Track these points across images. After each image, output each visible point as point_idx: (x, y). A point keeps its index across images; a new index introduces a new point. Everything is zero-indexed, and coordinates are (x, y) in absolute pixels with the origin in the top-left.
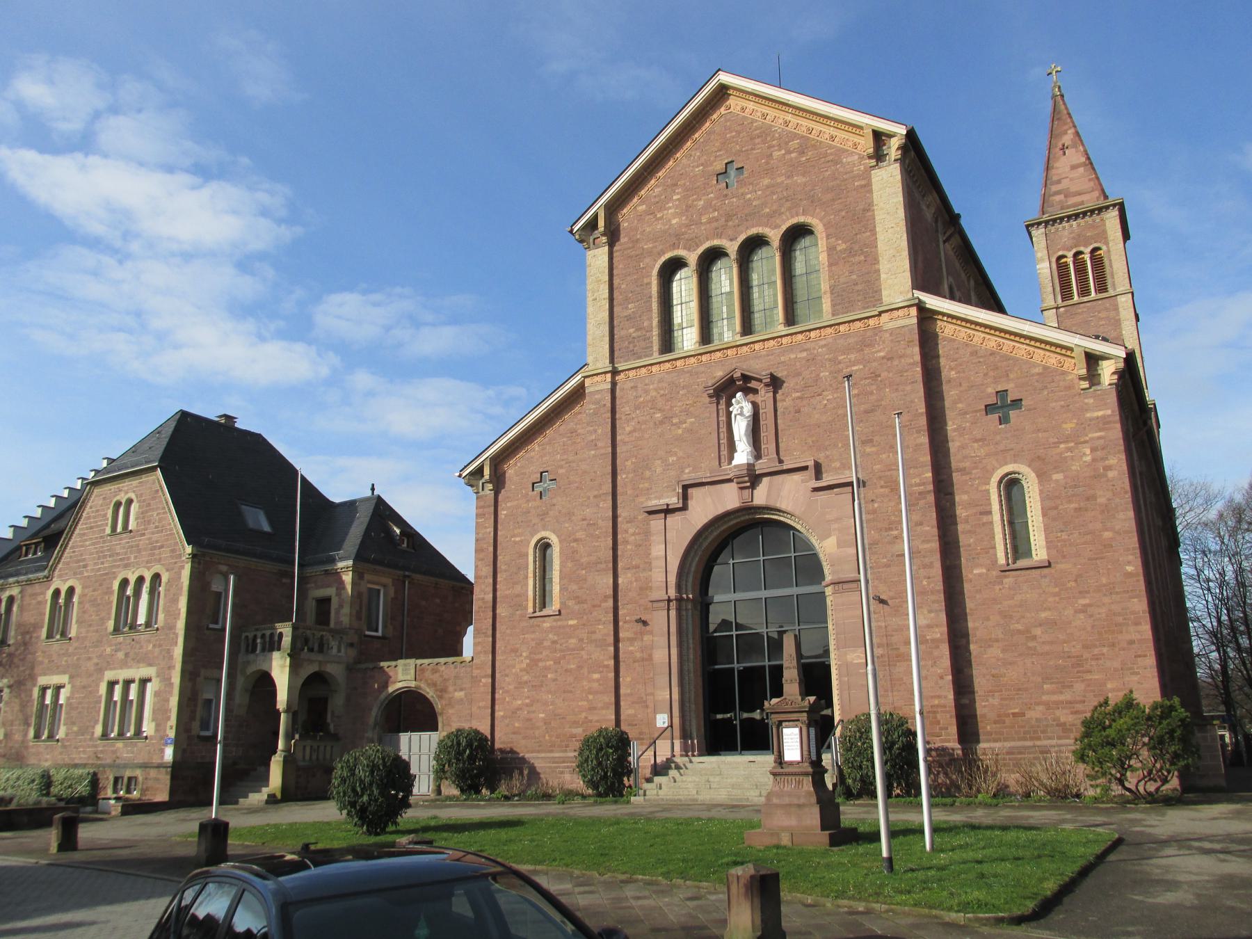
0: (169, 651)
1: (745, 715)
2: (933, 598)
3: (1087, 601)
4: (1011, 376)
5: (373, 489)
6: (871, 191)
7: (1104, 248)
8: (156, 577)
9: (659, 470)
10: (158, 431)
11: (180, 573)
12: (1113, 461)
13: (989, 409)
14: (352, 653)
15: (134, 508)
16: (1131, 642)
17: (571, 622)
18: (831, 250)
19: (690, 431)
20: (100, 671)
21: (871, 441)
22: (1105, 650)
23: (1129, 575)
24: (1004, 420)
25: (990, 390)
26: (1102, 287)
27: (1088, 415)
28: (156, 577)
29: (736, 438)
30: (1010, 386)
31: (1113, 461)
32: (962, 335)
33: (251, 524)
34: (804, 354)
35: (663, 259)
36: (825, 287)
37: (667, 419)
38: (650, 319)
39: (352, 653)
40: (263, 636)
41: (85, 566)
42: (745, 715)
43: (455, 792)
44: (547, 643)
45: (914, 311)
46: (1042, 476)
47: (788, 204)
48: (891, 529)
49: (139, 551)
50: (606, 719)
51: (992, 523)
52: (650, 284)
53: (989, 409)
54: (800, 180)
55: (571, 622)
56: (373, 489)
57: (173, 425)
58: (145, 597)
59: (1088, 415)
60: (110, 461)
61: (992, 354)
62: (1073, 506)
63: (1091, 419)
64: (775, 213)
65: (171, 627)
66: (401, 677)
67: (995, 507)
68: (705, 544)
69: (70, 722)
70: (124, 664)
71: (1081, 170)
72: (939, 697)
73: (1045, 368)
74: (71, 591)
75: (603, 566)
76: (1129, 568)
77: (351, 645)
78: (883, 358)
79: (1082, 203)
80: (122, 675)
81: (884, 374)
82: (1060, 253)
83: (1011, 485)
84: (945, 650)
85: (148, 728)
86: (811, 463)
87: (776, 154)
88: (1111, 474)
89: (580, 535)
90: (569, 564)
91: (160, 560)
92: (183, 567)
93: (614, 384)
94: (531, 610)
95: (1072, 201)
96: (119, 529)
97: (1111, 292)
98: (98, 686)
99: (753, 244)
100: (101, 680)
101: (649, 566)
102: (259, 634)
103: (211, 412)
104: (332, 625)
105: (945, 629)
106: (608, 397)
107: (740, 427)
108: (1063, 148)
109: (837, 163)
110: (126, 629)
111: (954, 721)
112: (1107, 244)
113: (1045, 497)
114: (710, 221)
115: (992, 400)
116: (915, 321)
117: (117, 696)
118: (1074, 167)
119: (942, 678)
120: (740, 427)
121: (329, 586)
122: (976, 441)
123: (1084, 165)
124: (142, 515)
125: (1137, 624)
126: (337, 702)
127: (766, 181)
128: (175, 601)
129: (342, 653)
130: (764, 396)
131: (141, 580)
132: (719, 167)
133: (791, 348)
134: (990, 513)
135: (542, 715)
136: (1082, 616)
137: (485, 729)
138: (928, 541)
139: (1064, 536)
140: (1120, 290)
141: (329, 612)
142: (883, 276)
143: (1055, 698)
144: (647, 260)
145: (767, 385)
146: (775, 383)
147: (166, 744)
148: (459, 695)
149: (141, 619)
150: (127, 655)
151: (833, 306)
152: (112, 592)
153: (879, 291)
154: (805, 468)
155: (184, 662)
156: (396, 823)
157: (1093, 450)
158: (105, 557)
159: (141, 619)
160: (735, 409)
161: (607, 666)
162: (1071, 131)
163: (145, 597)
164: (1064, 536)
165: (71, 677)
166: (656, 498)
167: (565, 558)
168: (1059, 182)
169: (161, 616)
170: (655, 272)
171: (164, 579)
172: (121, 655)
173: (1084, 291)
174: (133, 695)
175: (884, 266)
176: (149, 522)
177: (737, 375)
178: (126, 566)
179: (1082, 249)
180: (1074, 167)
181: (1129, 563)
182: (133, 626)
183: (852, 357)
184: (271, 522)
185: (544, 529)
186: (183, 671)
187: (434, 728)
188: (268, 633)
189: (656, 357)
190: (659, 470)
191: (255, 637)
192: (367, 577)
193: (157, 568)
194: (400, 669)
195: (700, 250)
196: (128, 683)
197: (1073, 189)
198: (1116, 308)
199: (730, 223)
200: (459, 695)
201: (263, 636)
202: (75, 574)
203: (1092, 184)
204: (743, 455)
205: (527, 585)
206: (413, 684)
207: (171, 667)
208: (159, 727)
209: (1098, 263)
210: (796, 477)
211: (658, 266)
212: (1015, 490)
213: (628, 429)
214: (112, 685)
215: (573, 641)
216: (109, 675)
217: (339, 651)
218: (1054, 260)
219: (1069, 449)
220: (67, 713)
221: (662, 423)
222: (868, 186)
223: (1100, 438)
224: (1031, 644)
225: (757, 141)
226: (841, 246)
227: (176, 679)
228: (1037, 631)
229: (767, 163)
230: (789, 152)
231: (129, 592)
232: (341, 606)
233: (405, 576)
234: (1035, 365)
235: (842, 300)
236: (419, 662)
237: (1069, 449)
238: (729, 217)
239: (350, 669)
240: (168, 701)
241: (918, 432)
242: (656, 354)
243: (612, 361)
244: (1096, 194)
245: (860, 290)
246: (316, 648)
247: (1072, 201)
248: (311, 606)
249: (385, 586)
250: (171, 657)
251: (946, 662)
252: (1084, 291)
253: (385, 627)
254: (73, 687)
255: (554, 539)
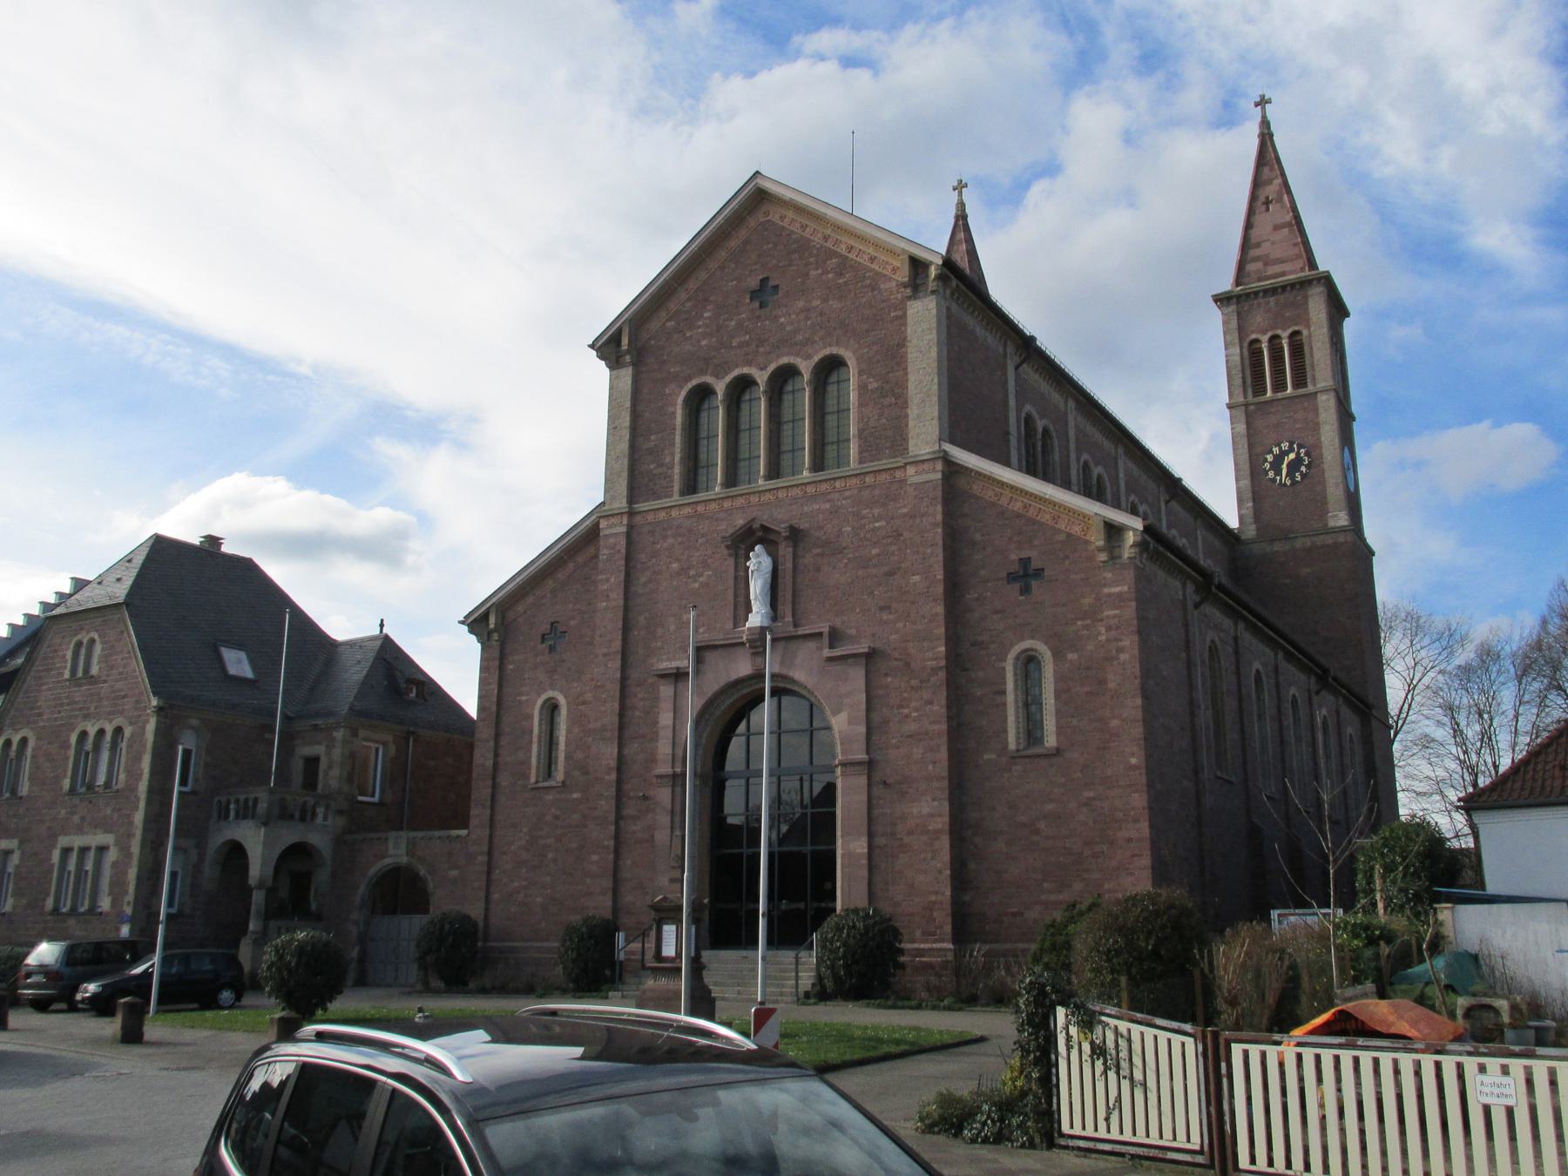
0: (128, 816)
1: (802, 905)
2: (936, 784)
3: (1091, 794)
4: (1036, 543)
5: (382, 625)
6: (905, 324)
7: (1305, 332)
8: (118, 731)
9: (672, 628)
10: (129, 559)
11: (144, 728)
12: (1126, 643)
13: (1012, 578)
14: (341, 822)
15: (98, 648)
16: (1129, 840)
17: (575, 796)
18: (862, 388)
19: (705, 585)
20: (53, 837)
21: (889, 607)
22: (1105, 848)
23: (1134, 768)
24: (1026, 590)
25: (1013, 557)
26: (1300, 380)
27: (1106, 590)
28: (118, 731)
29: (752, 597)
30: (1033, 554)
31: (1126, 643)
32: (991, 493)
33: (243, 655)
34: (828, 505)
35: (690, 386)
36: (853, 430)
37: (684, 570)
38: (673, 454)
39: (341, 822)
40: (237, 801)
41: (40, 715)
42: (802, 905)
43: (442, 985)
44: (548, 818)
45: (939, 466)
46: (1058, 655)
47: (821, 333)
48: (901, 707)
49: (100, 700)
50: (601, 906)
51: (1005, 704)
52: (674, 413)
53: (1012, 578)
54: (835, 304)
55: (575, 796)
56: (382, 625)
57: (139, 560)
58: (105, 756)
59: (1106, 590)
60: (80, 584)
61: (1019, 516)
62: (1087, 689)
63: (1110, 595)
64: (809, 342)
65: (131, 788)
66: (391, 851)
67: (1010, 686)
68: (718, 713)
69: (18, 894)
70: (80, 830)
71: (1286, 231)
72: (936, 893)
73: (1069, 535)
74: (24, 741)
75: (609, 734)
76: (1133, 761)
77: (340, 812)
78: (906, 515)
79: (1283, 274)
80: (78, 841)
81: (906, 534)
82: (1253, 336)
83: (1029, 662)
84: (945, 843)
85: (105, 904)
86: (826, 630)
87: (813, 273)
88: (1123, 657)
89: (589, 696)
90: (576, 730)
91: (122, 712)
92: (147, 721)
93: (631, 527)
94: (533, 780)
95: (1271, 270)
96: (80, 673)
97: (1311, 388)
98: (50, 853)
99: (786, 374)
100: (53, 846)
101: (655, 737)
102: (232, 799)
103: (189, 533)
104: (320, 787)
105: (946, 819)
106: (623, 542)
107: (757, 587)
108: (1267, 202)
109: (873, 289)
110: (83, 790)
111: (949, 920)
112: (1308, 327)
113: (1060, 679)
114: (740, 346)
115: (1015, 567)
116: (939, 476)
117: (72, 867)
118: (1276, 228)
119: (940, 872)
120: (757, 587)
121: (319, 743)
122: (997, 612)
123: (1289, 225)
124: (105, 658)
125: (1136, 821)
126: (322, 877)
127: (801, 304)
128: (138, 759)
129: (329, 822)
130: (785, 551)
131: (101, 732)
132: (754, 282)
133: (814, 497)
134: (1004, 693)
135: (539, 900)
136: (1085, 810)
137: (475, 911)
138: (935, 722)
139: (1075, 722)
140: (1321, 385)
141: (316, 774)
142: (911, 423)
143: (1053, 897)
144: (673, 386)
145: (786, 538)
146: (795, 535)
147: (123, 922)
148: (454, 873)
149: (101, 779)
150: (83, 819)
151: (860, 453)
152: (69, 746)
153: (906, 440)
154: (820, 634)
155: (145, 830)
156: (325, 1010)
157: (1109, 629)
158: (62, 705)
159: (101, 779)
160: (752, 564)
161: (607, 847)
162: (1279, 181)
163: (105, 756)
164: (1075, 722)
165: (21, 842)
166: (669, 660)
167: (573, 720)
168: (1258, 245)
169: (122, 777)
170: (680, 400)
171: (128, 732)
172: (76, 819)
173: (1279, 385)
174: (89, 866)
175: (913, 412)
176: (112, 667)
177: (756, 526)
178: (86, 717)
179: (1279, 332)
180: (1276, 228)
181: (1133, 755)
182: (90, 787)
183: (876, 511)
184: (254, 668)
185: (552, 687)
186: (144, 840)
187: (425, 911)
188: (242, 797)
189: (676, 498)
190: (672, 628)
191: (228, 803)
192: (362, 733)
193: (119, 721)
194: (391, 844)
195: (728, 379)
196: (84, 850)
197: (1272, 256)
198: (1316, 411)
199: (761, 349)
200: (454, 873)
201: (237, 801)
202: (29, 723)
203: (1296, 250)
204: (757, 617)
205: (530, 751)
206: (404, 860)
207: (130, 835)
208: (115, 902)
209: (1298, 350)
210: (812, 645)
211: (683, 393)
212: (1032, 666)
213: (643, 579)
214: (66, 851)
215: (576, 817)
216: (63, 841)
217: (325, 818)
218: (1246, 345)
219: (1086, 627)
220: (15, 883)
221: (678, 574)
222: (903, 318)
223: (1115, 616)
224: (1035, 838)
225: (796, 256)
226: (873, 385)
227: (136, 849)
228: (1042, 825)
229: (803, 283)
230: (826, 272)
231: (89, 746)
232: (330, 767)
233: (409, 733)
234: (1059, 531)
235: (869, 449)
236: (413, 834)
237: (1086, 627)
238: (761, 342)
239: (339, 842)
240: (126, 873)
241: (935, 600)
242: (676, 496)
243: (631, 500)
244: (1300, 263)
245: (888, 437)
246: (297, 815)
247: (1271, 270)
248: (298, 766)
249: (385, 744)
250: (131, 823)
251: (945, 855)
252: (1279, 385)
253: (383, 790)
254: (23, 854)
255: (562, 700)
